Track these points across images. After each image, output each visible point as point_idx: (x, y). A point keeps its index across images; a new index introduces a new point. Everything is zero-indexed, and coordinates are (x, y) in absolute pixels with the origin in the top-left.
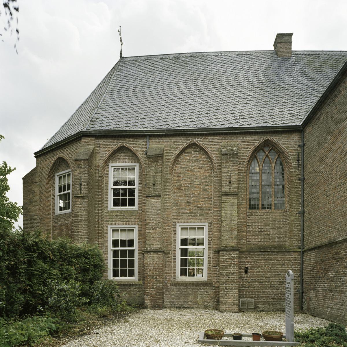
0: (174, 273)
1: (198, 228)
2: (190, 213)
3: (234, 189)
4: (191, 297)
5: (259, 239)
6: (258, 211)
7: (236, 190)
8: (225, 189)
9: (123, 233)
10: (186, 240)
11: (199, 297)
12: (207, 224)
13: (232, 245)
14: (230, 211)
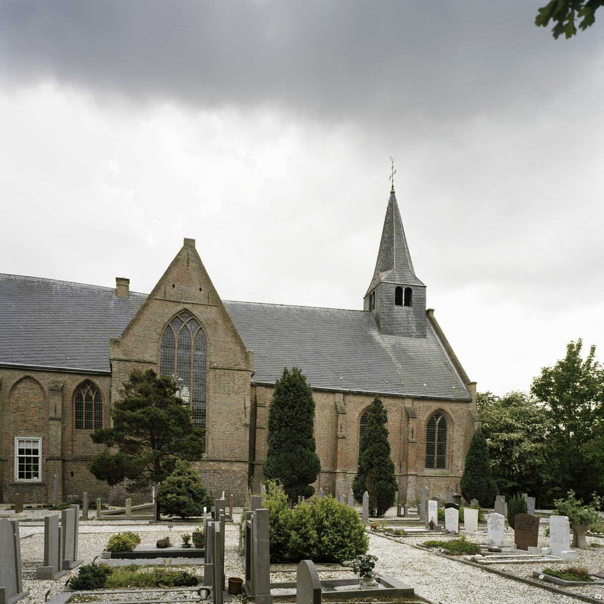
0: (13, 476)
1: (33, 441)
2: (26, 429)
3: (59, 415)
4: (27, 495)
5: (82, 451)
6: (81, 430)
7: (60, 416)
8: (52, 415)
9: (29, 444)
10: (23, 450)
11: (34, 495)
12: (41, 438)
13: (57, 455)
14: (55, 431)
